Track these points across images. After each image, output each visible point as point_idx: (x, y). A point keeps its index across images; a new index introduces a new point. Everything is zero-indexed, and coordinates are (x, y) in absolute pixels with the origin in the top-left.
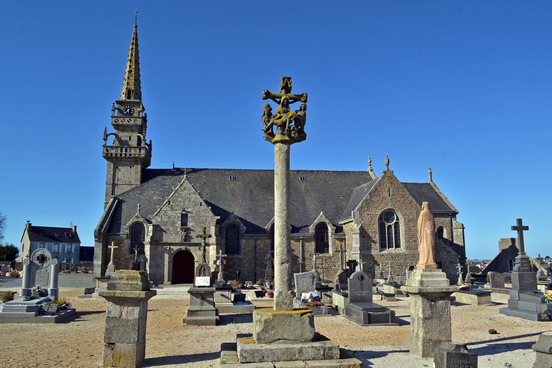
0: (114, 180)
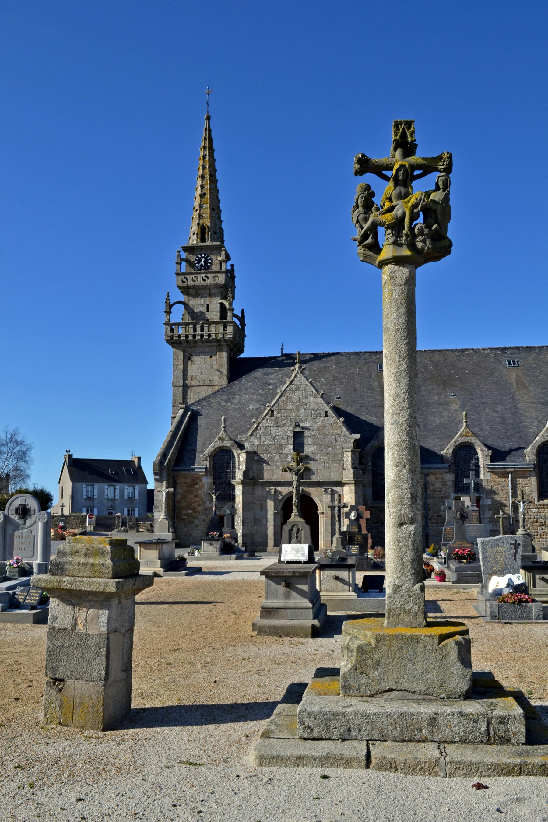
0: (185, 379)
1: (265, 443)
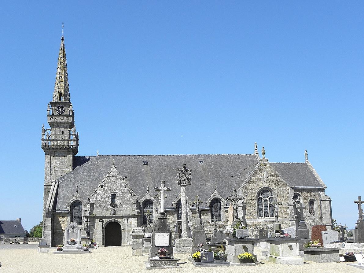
1: (99, 199)
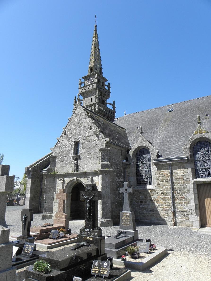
1: (61, 151)
